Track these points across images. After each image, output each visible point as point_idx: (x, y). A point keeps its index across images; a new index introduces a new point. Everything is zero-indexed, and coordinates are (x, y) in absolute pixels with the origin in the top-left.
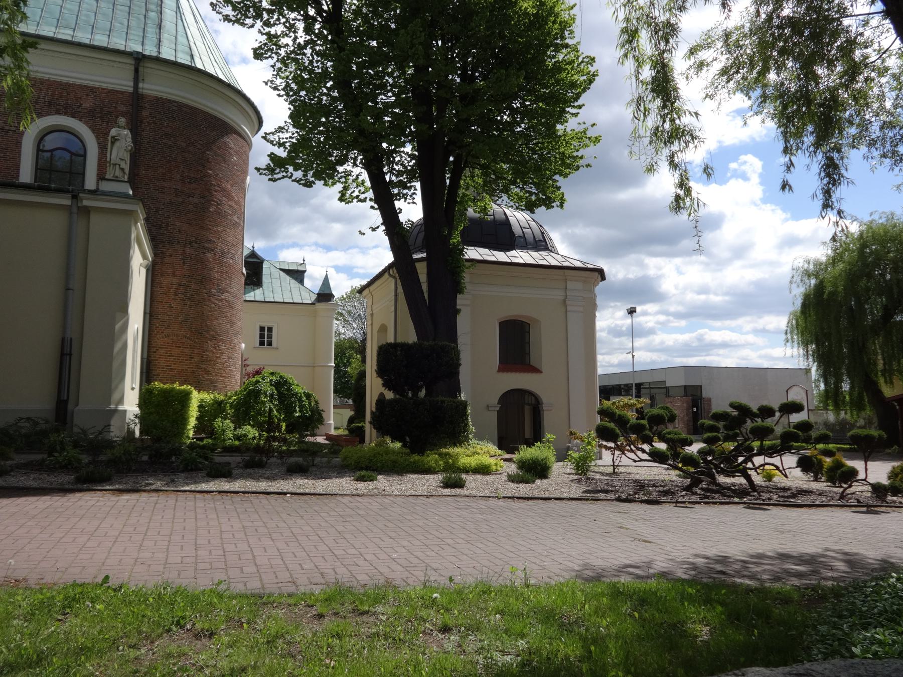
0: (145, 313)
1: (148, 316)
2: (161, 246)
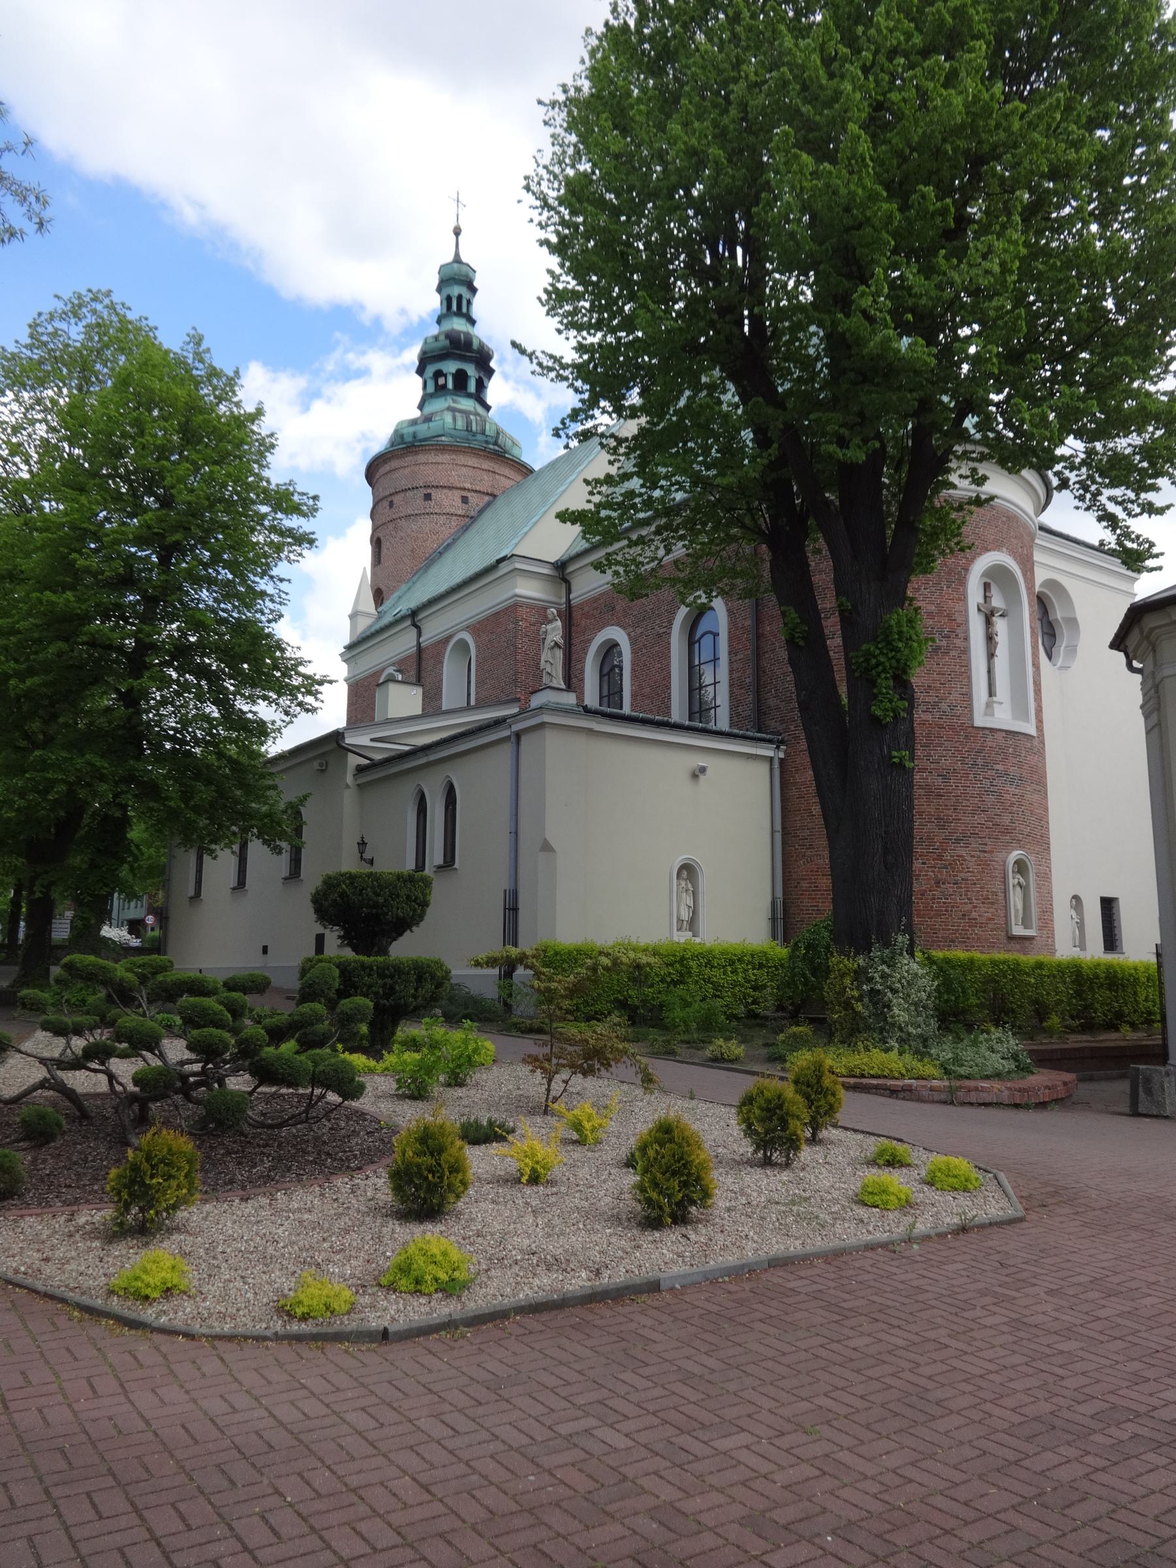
0: (773, 919)
1: (778, 837)
2: (792, 728)
